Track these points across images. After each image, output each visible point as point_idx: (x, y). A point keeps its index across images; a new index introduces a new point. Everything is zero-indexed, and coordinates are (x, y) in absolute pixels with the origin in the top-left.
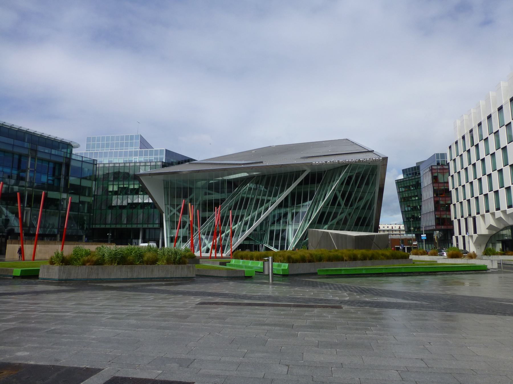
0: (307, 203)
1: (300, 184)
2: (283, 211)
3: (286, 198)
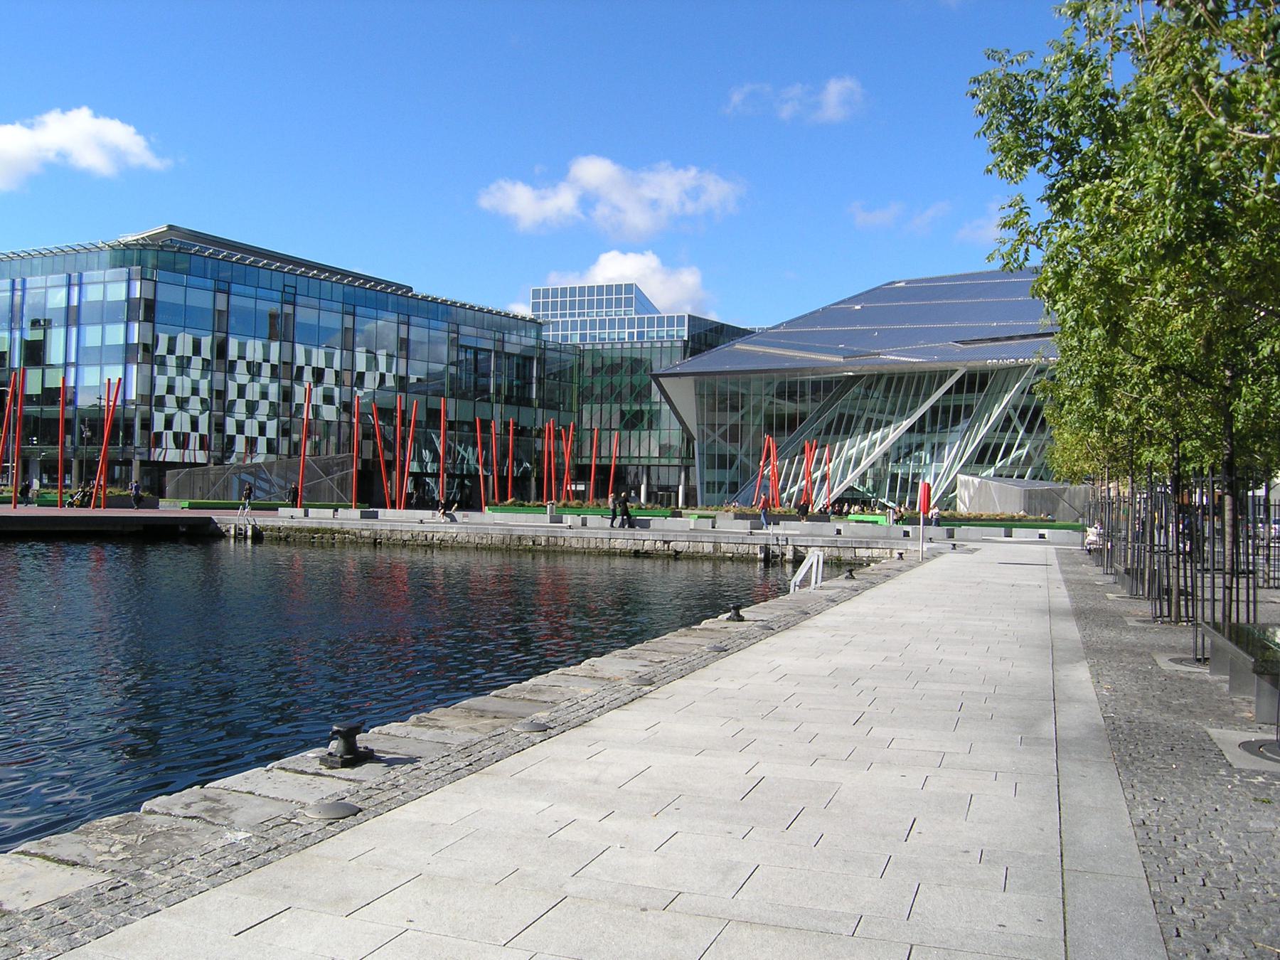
0: (958, 428)
1: (948, 392)
2: (915, 438)
3: (923, 418)
